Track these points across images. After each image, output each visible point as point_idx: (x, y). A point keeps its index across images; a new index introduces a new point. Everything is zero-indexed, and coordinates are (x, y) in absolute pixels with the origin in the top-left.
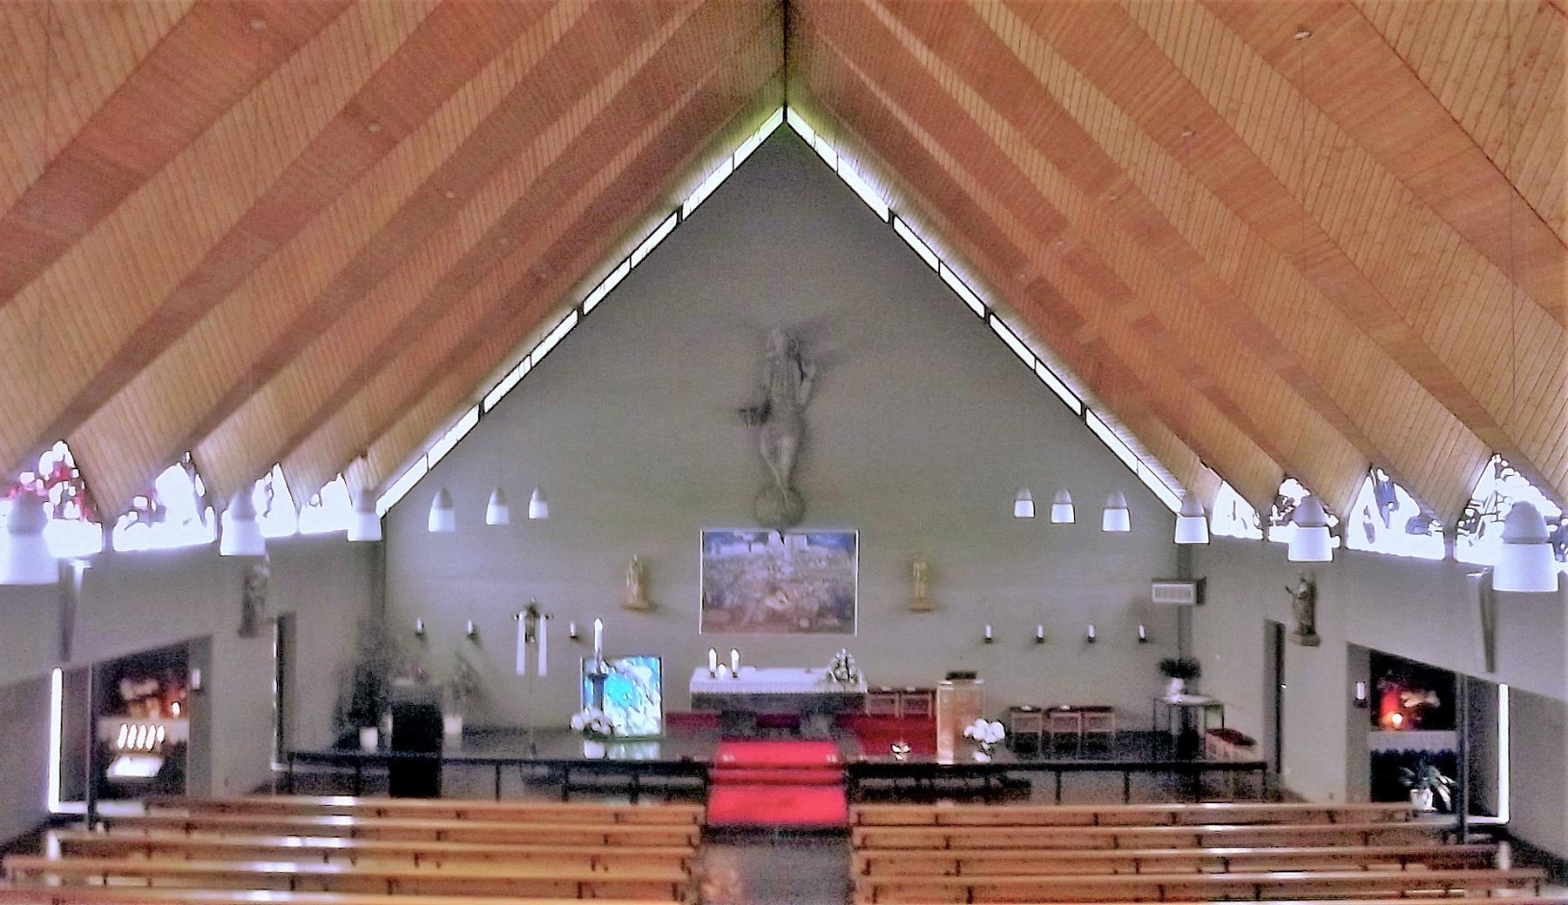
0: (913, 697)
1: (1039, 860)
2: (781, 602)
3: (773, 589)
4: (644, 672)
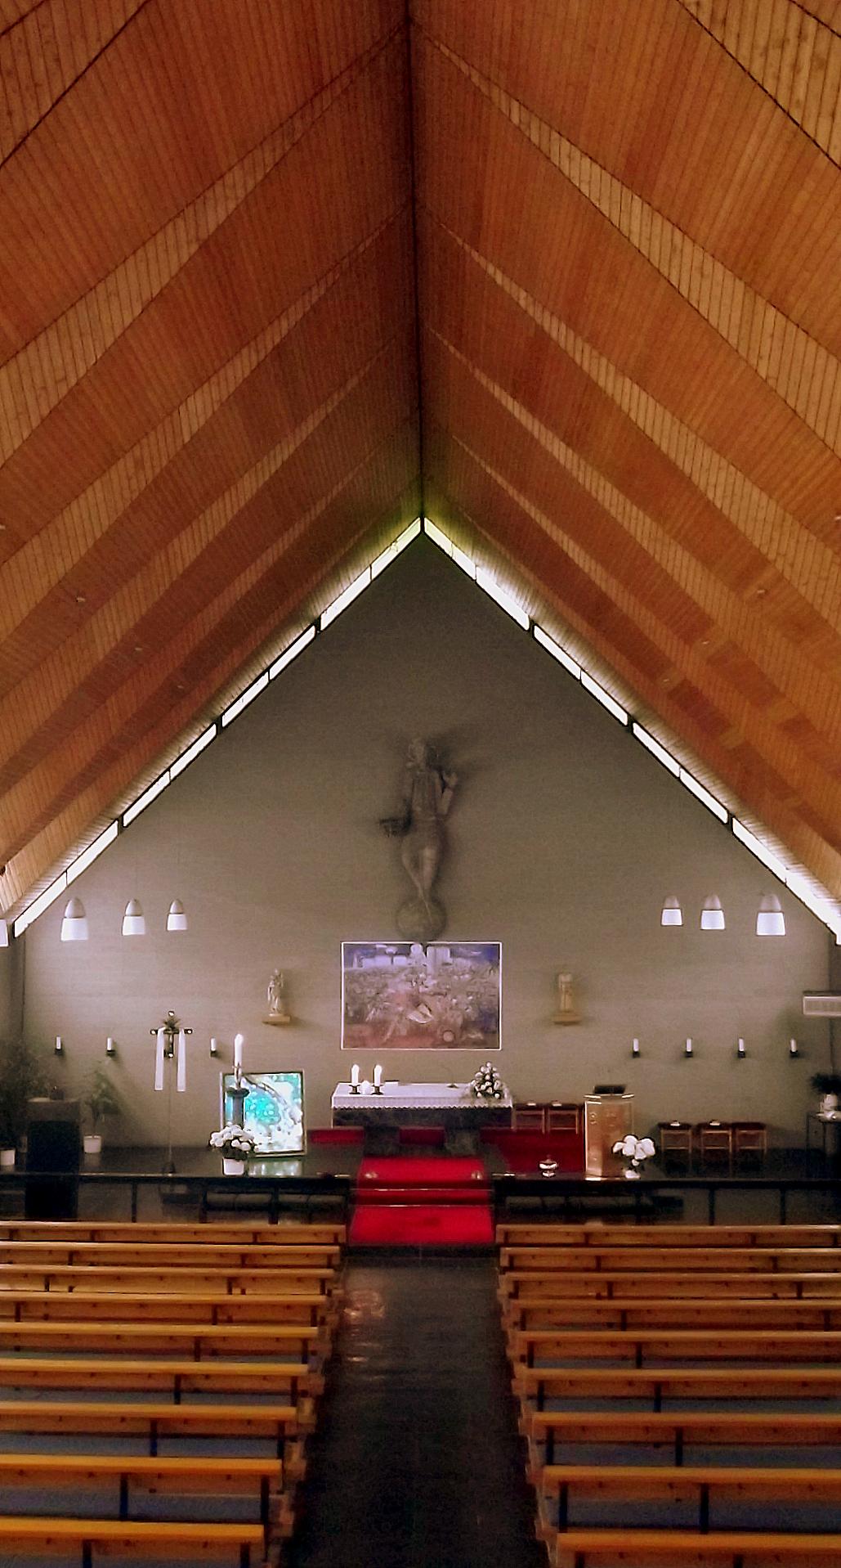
0: (557, 1112)
1: (691, 1282)
2: (425, 1016)
3: (416, 1002)
4: (285, 1090)
